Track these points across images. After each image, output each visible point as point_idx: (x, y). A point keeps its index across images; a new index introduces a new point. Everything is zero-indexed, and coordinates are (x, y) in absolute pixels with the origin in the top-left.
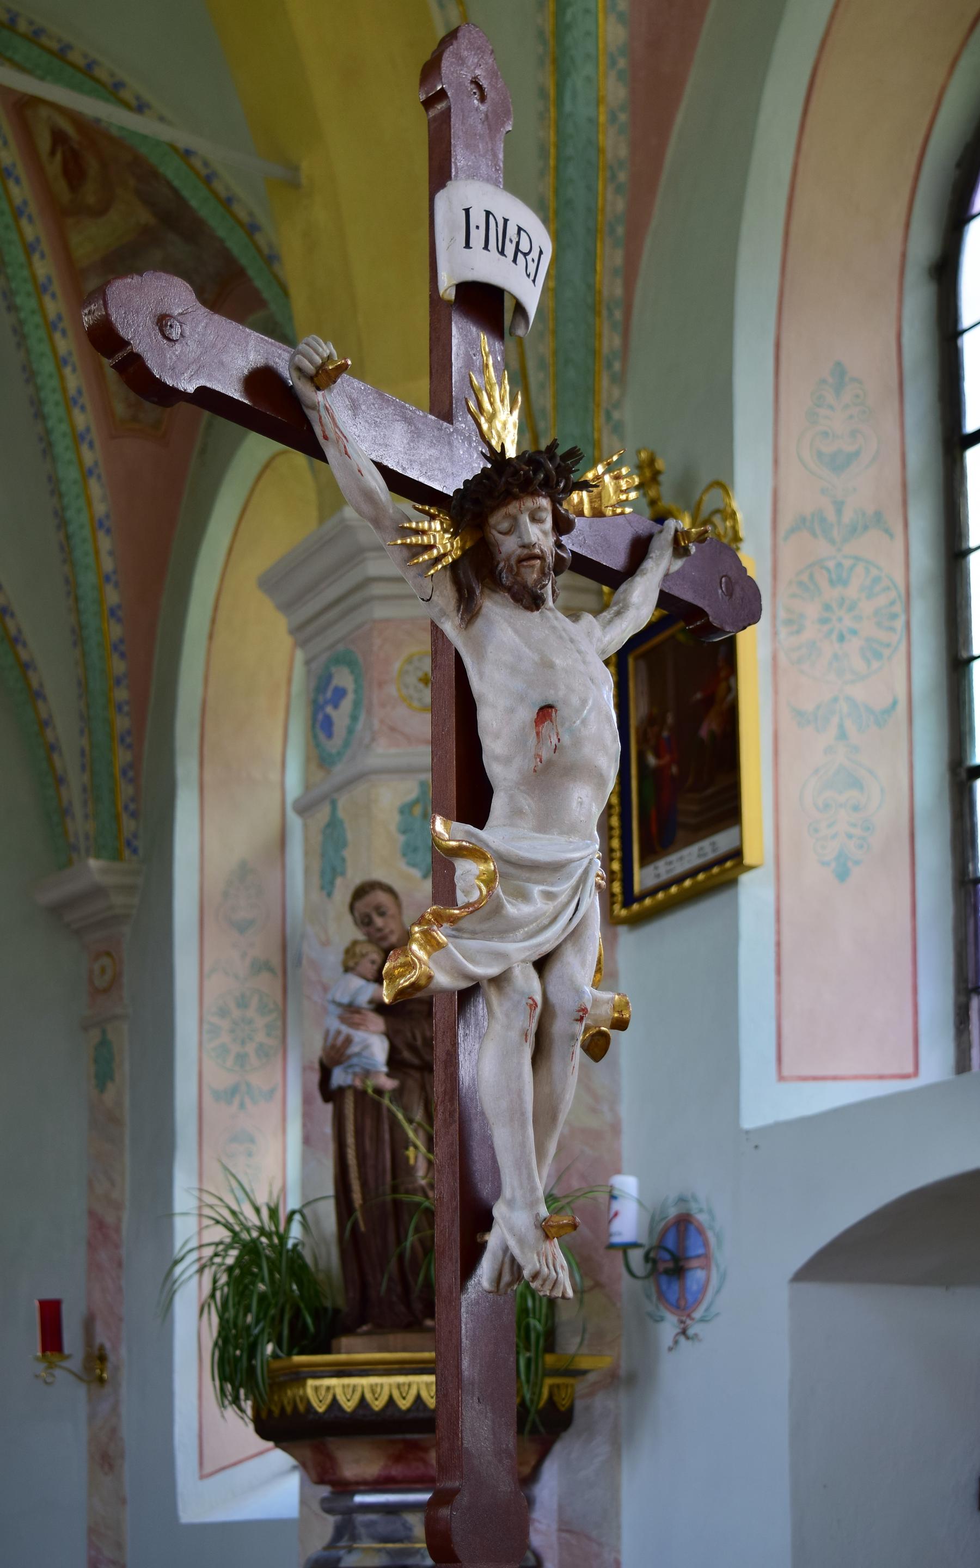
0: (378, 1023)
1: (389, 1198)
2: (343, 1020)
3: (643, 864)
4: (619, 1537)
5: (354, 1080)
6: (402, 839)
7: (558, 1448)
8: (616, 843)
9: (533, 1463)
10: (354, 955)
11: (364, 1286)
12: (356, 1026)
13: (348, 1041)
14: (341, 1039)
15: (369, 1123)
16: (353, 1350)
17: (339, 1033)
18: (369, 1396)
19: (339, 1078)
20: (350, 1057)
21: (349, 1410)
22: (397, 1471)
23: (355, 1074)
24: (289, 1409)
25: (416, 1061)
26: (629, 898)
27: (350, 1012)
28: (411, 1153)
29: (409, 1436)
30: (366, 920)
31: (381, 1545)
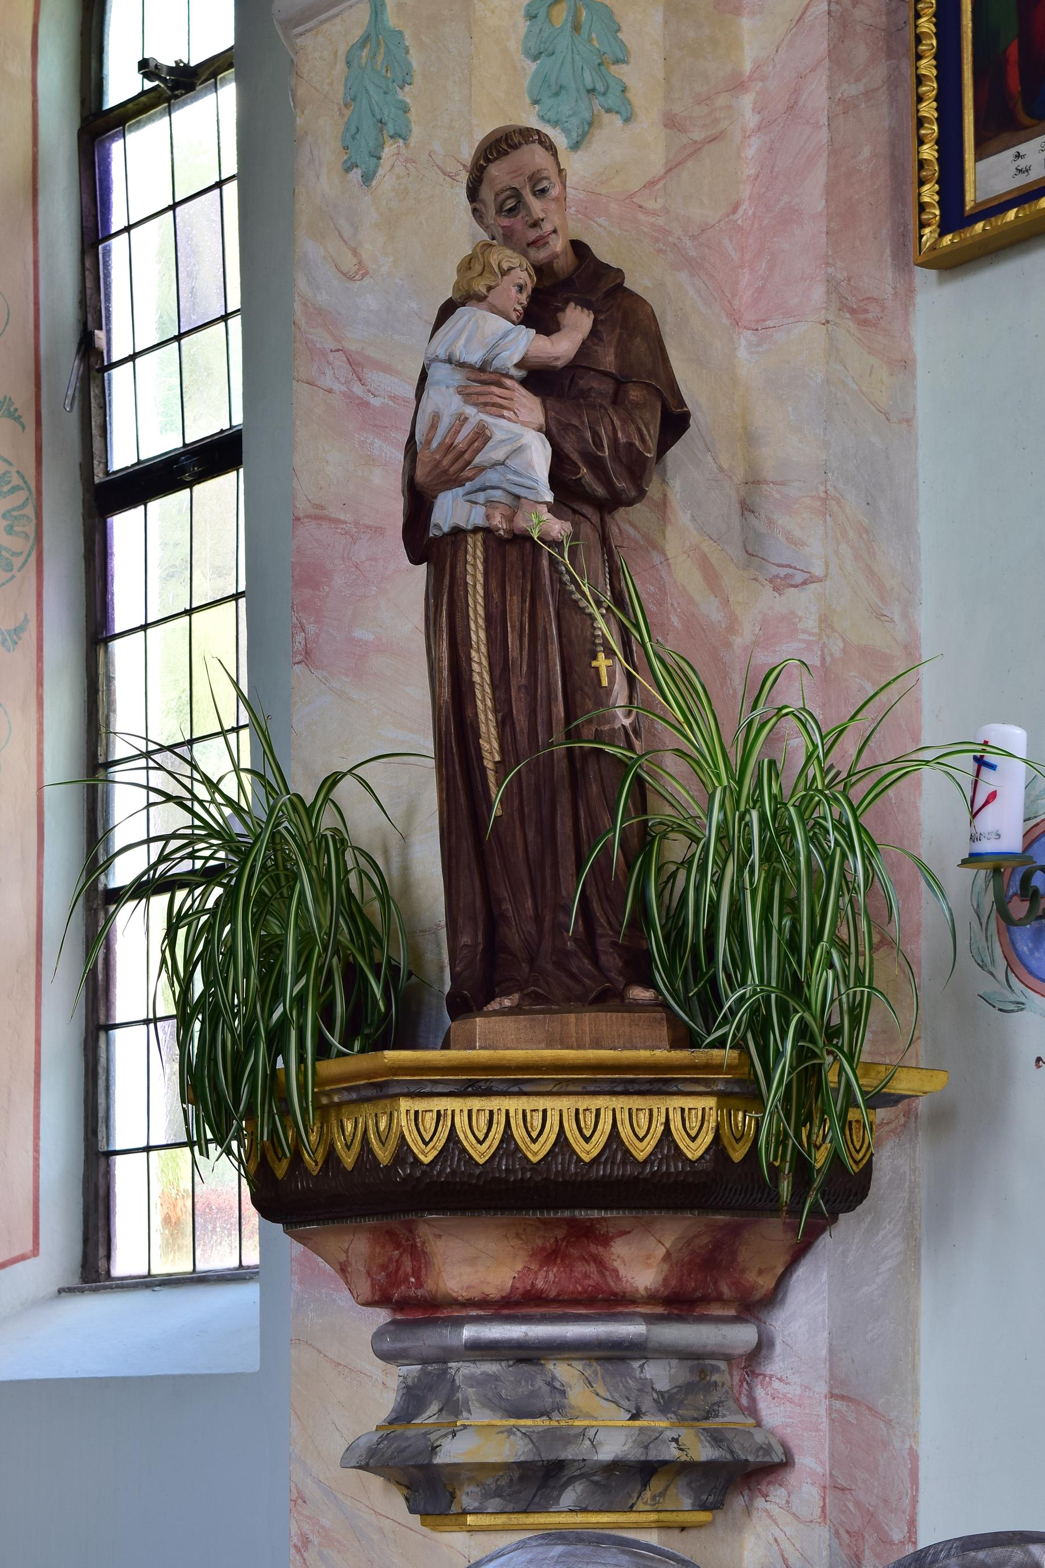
0: (530, 407)
1: (560, 749)
2: (467, 395)
3: (980, 155)
4: (916, 1412)
5: (488, 517)
6: (406, 95)
7: (826, 1242)
8: (929, 109)
9: (780, 1270)
10: (486, 267)
11: (493, 922)
12: (497, 408)
13: (482, 437)
14: (466, 431)
15: (514, 603)
16: (191, 1092)
17: (463, 420)
18: (519, 1133)
19: (450, 511)
20: (481, 469)
21: (481, 1161)
22: (547, 1279)
23: (489, 503)
24: (348, 1160)
25: (600, 491)
26: (954, 216)
27: (482, 378)
28: (602, 662)
29: (581, 1214)
30: (510, 204)
31: (512, 1422)
